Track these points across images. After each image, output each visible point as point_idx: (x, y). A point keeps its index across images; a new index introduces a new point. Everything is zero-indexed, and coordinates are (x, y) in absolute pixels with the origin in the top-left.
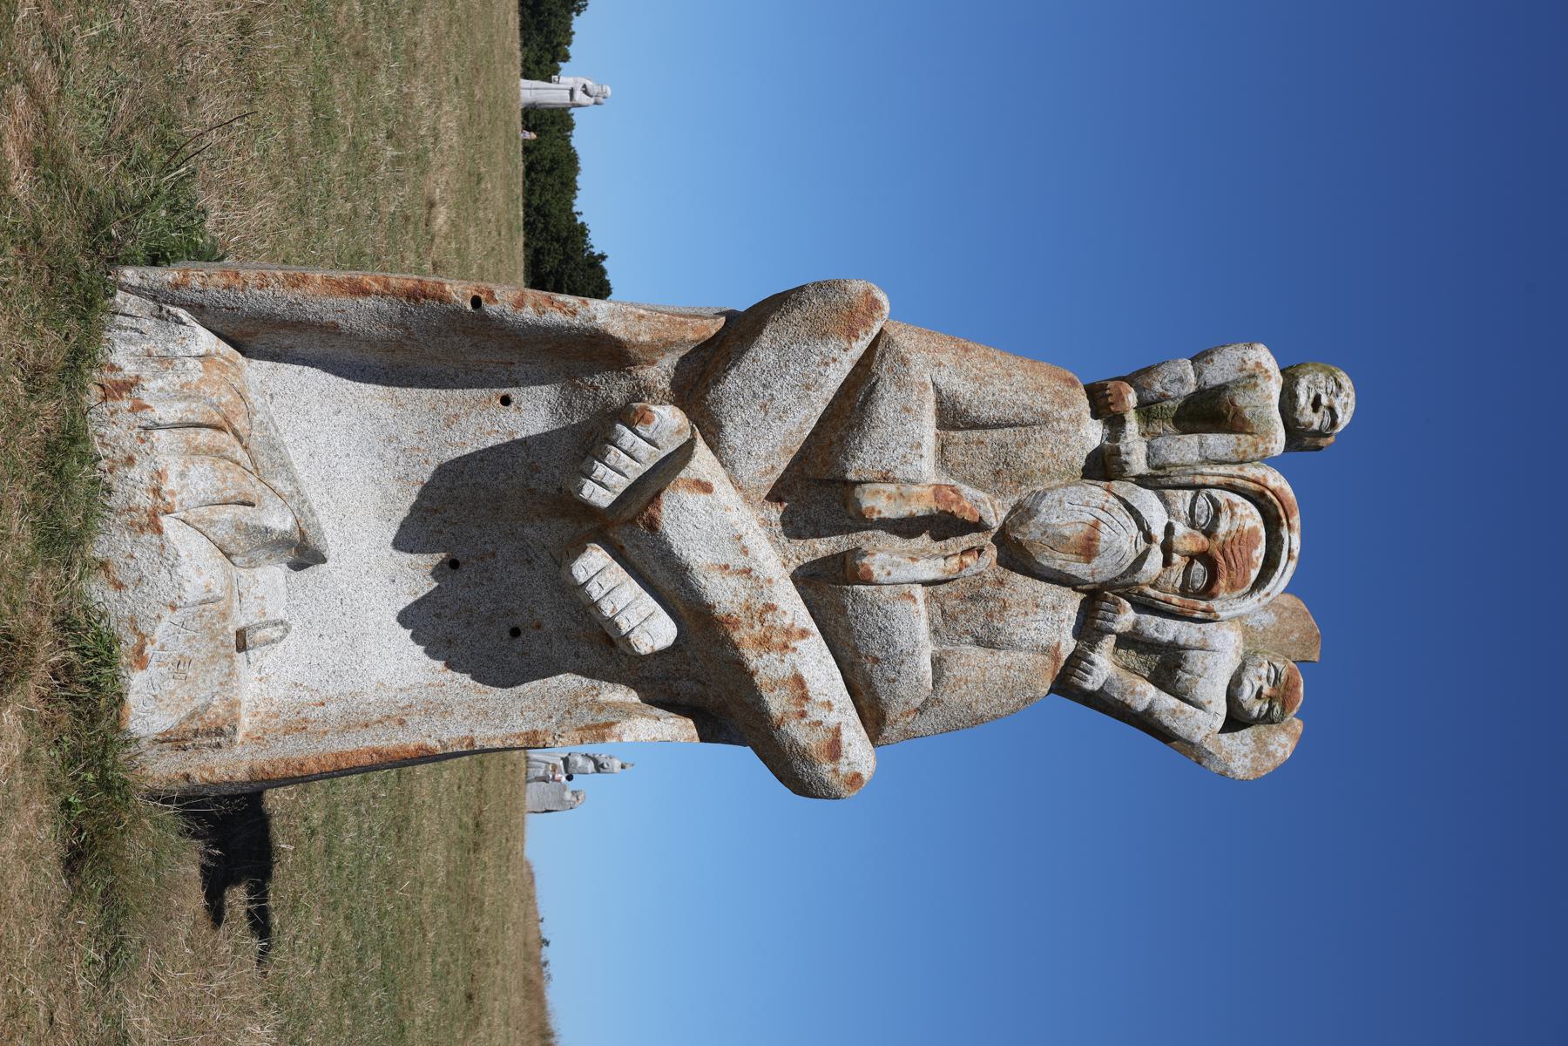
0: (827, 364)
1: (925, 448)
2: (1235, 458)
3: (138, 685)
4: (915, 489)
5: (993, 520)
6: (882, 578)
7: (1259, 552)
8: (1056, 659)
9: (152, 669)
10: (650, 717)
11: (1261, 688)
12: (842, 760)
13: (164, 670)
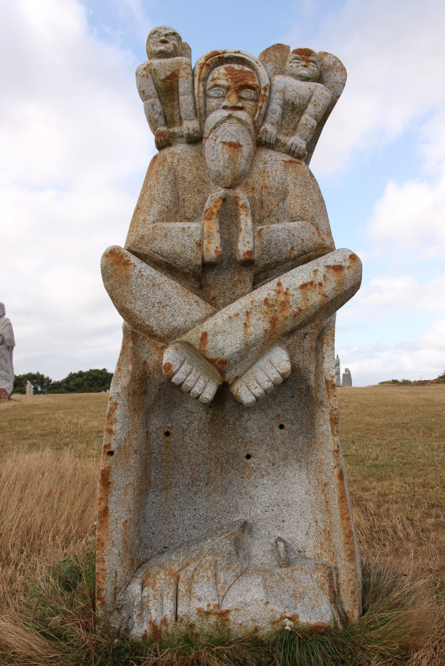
0: (142, 275)
1: (185, 226)
2: (190, 78)
3: (307, 619)
4: (205, 230)
5: (221, 192)
6: (251, 245)
7: (236, 67)
8: (290, 162)
9: (298, 611)
10: (323, 362)
11: (302, 65)
12: (343, 264)
13: (299, 605)
